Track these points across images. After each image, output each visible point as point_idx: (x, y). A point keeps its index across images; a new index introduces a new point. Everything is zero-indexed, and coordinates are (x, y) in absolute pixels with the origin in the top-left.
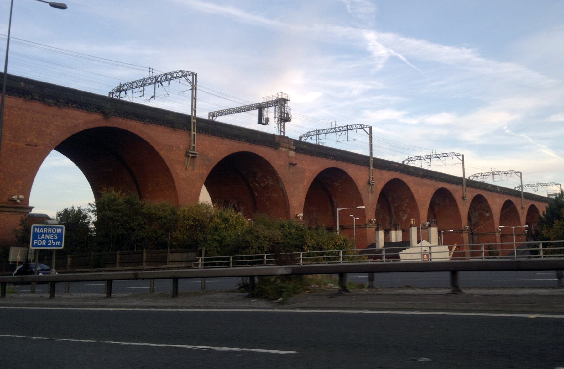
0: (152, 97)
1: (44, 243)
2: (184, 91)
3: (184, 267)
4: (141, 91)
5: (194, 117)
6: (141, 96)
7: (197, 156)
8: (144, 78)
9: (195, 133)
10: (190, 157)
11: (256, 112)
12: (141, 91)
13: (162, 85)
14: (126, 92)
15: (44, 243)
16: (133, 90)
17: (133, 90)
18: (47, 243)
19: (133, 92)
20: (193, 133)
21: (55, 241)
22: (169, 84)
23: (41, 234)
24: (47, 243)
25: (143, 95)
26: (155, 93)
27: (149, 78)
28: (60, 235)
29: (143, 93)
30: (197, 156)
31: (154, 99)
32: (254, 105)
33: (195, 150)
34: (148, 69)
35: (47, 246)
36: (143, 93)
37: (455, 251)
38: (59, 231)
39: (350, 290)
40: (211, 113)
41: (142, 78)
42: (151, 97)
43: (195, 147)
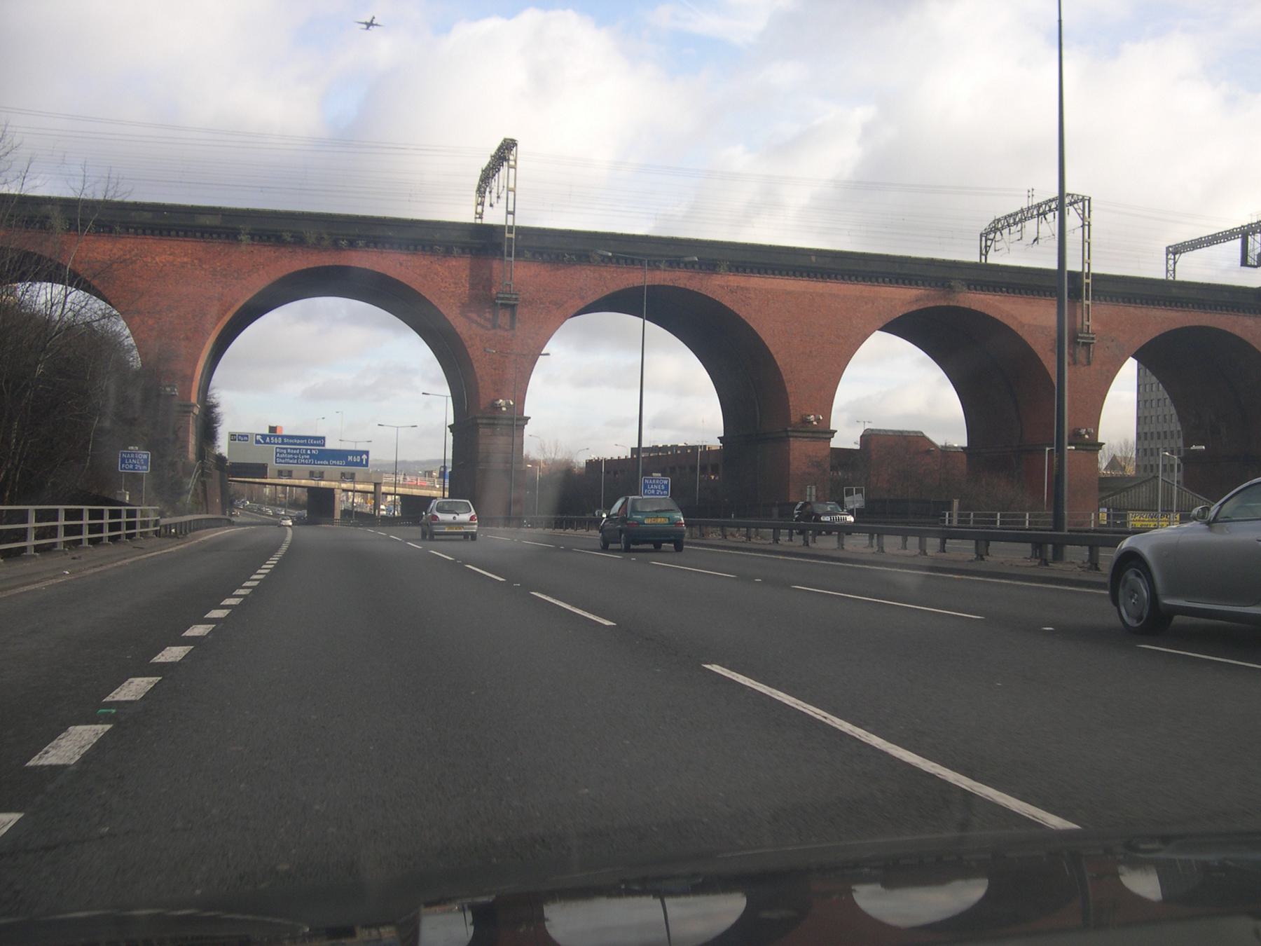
0: (1035, 241)
1: (131, 466)
2: (1074, 230)
3: (429, 486)
4: (1018, 231)
5: (1086, 273)
6: (1019, 240)
7: (1095, 341)
8: (1022, 209)
9: (1089, 302)
10: (1081, 344)
11: (1237, 243)
12: (1018, 231)
13: (1046, 219)
14: (1003, 232)
15: (131, 466)
16: (1010, 230)
17: (1010, 230)
18: (134, 467)
19: (1010, 233)
20: (1086, 302)
21: (662, 490)
22: (1002, 235)
23: (650, 485)
24: (134, 467)
25: (1021, 238)
26: (1038, 233)
27: (1029, 208)
28: (666, 486)
29: (1022, 234)
30: (1095, 341)
31: (1038, 243)
32: (1221, 235)
33: (1090, 332)
34: (1026, 193)
35: (656, 495)
36: (1022, 234)
37: (1213, 503)
38: (666, 482)
39: (1101, 569)
40: (1170, 247)
41: (1020, 209)
42: (1033, 240)
43: (366, 468)
